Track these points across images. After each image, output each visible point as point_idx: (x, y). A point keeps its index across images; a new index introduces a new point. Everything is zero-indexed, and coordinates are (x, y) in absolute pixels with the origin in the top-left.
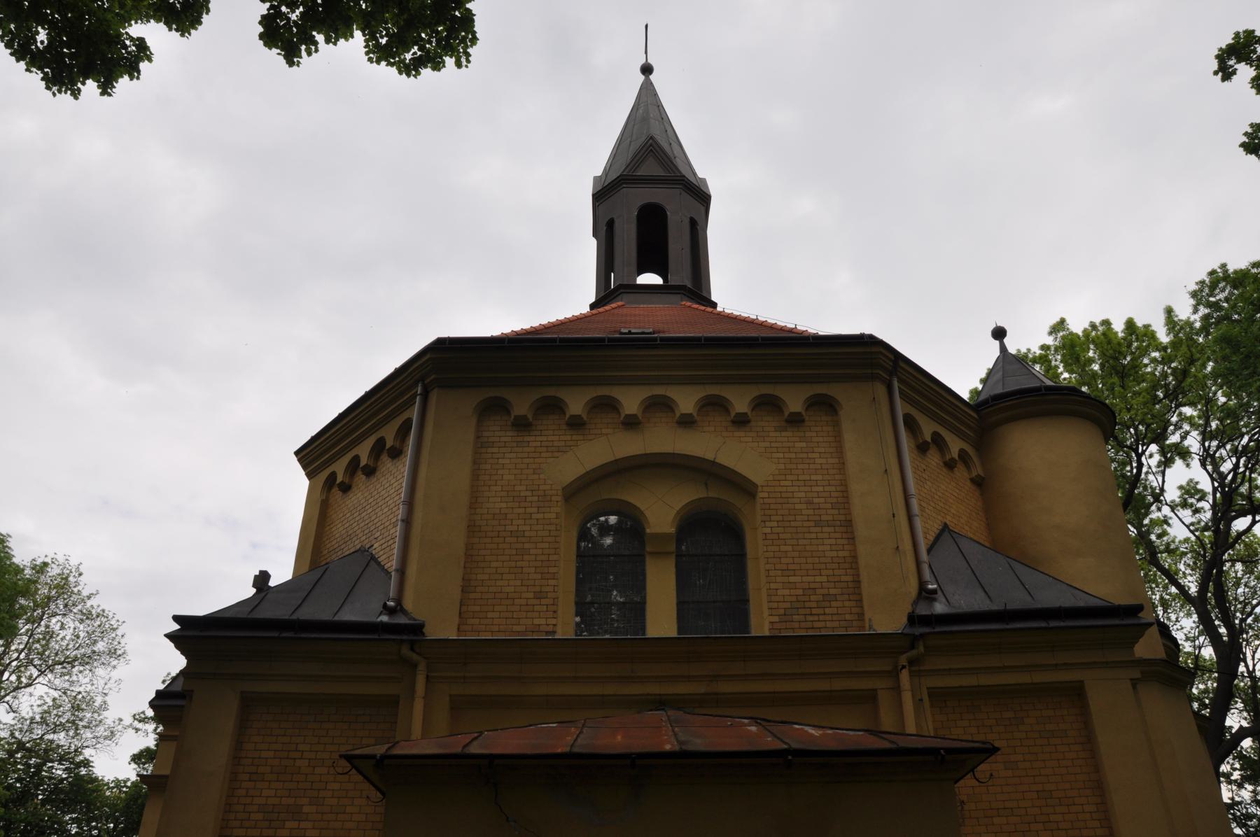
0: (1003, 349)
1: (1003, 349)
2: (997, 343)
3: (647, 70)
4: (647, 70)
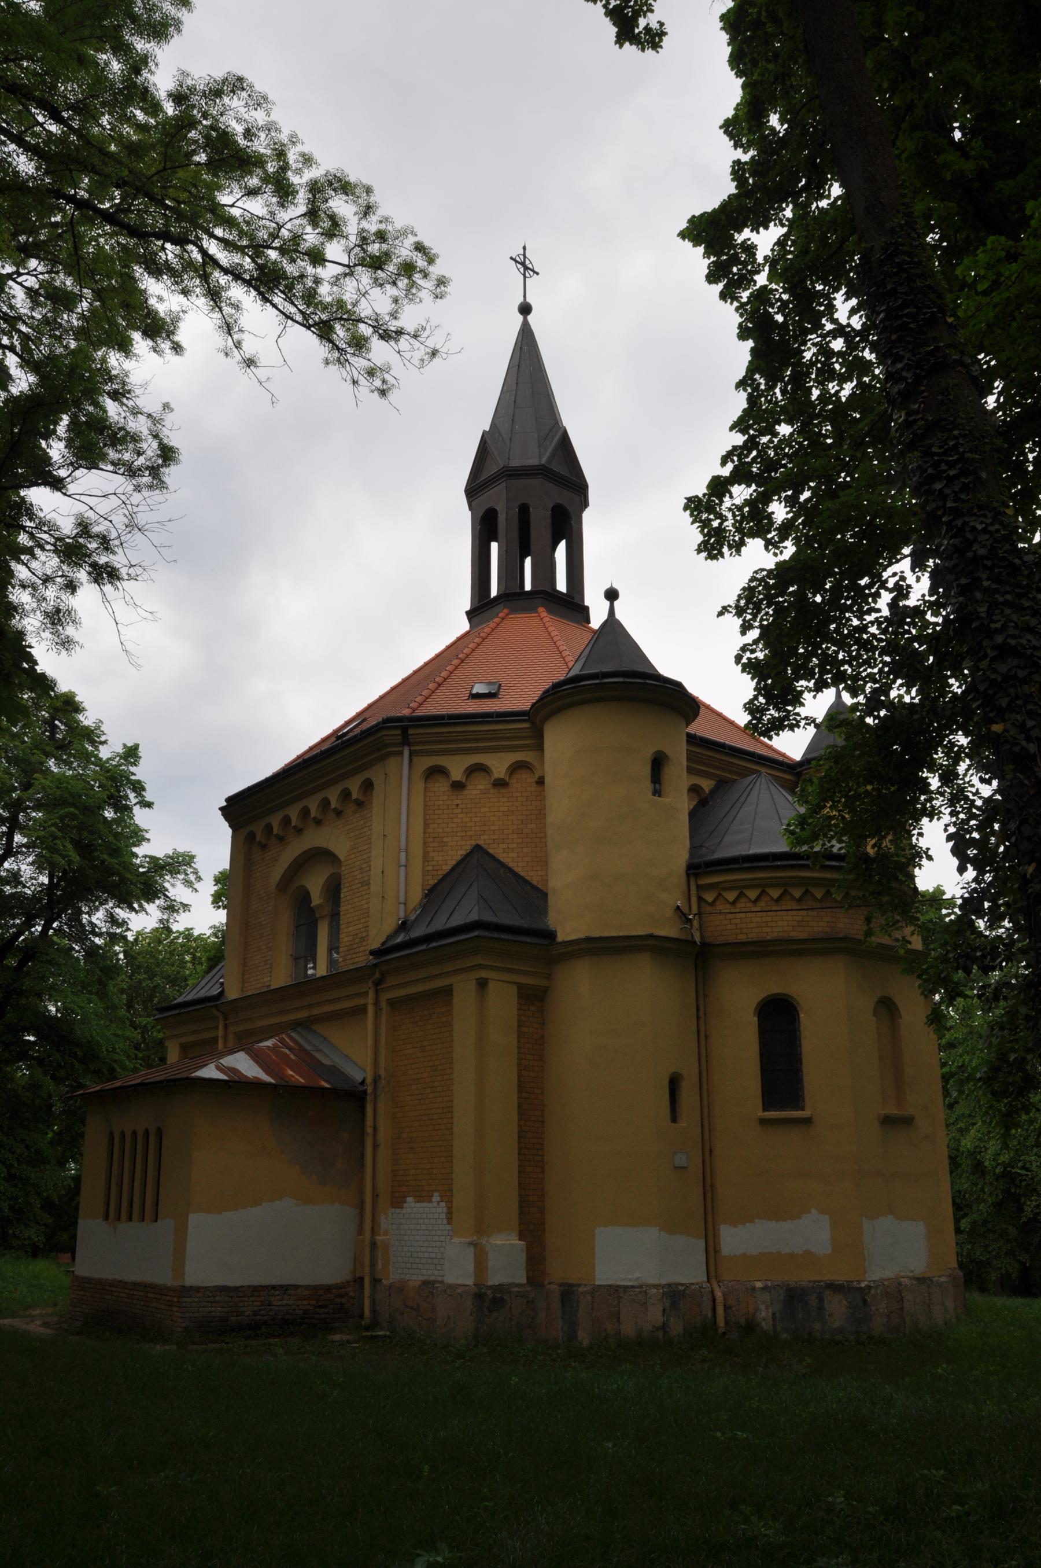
0: (612, 612)
1: (612, 612)
2: (608, 603)
3: (525, 309)
4: (525, 309)
